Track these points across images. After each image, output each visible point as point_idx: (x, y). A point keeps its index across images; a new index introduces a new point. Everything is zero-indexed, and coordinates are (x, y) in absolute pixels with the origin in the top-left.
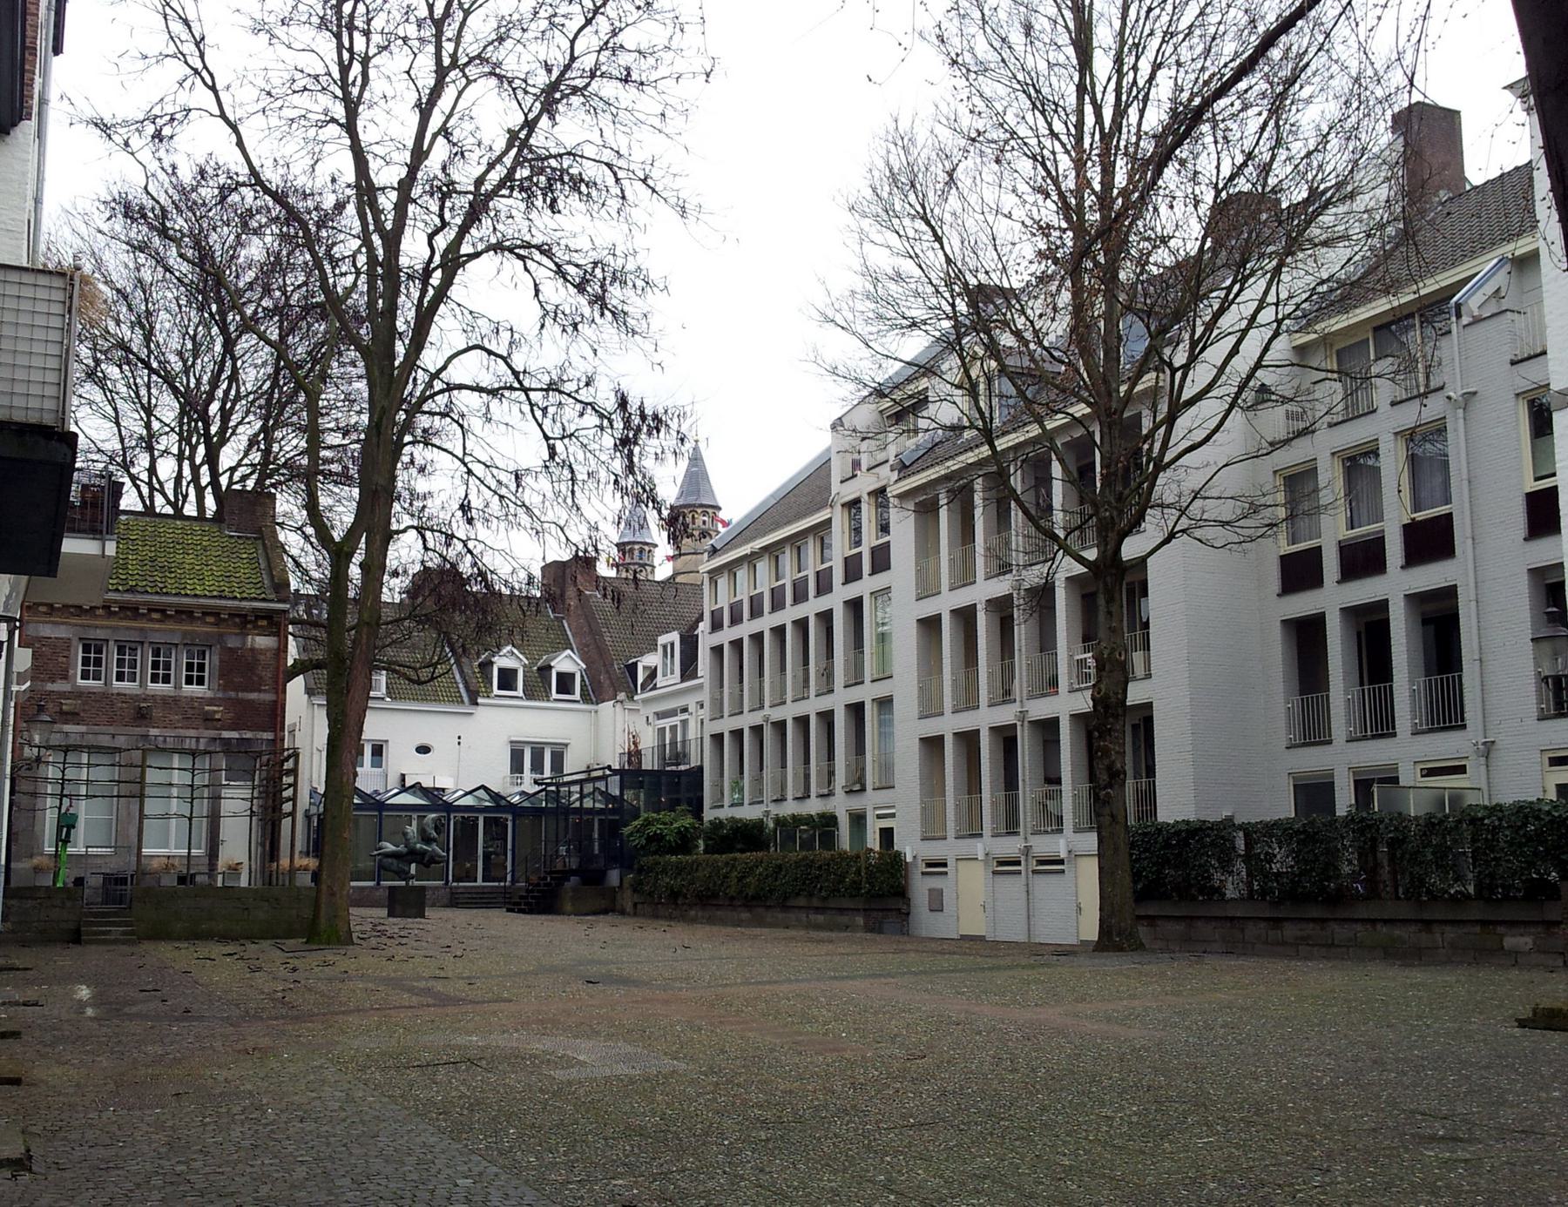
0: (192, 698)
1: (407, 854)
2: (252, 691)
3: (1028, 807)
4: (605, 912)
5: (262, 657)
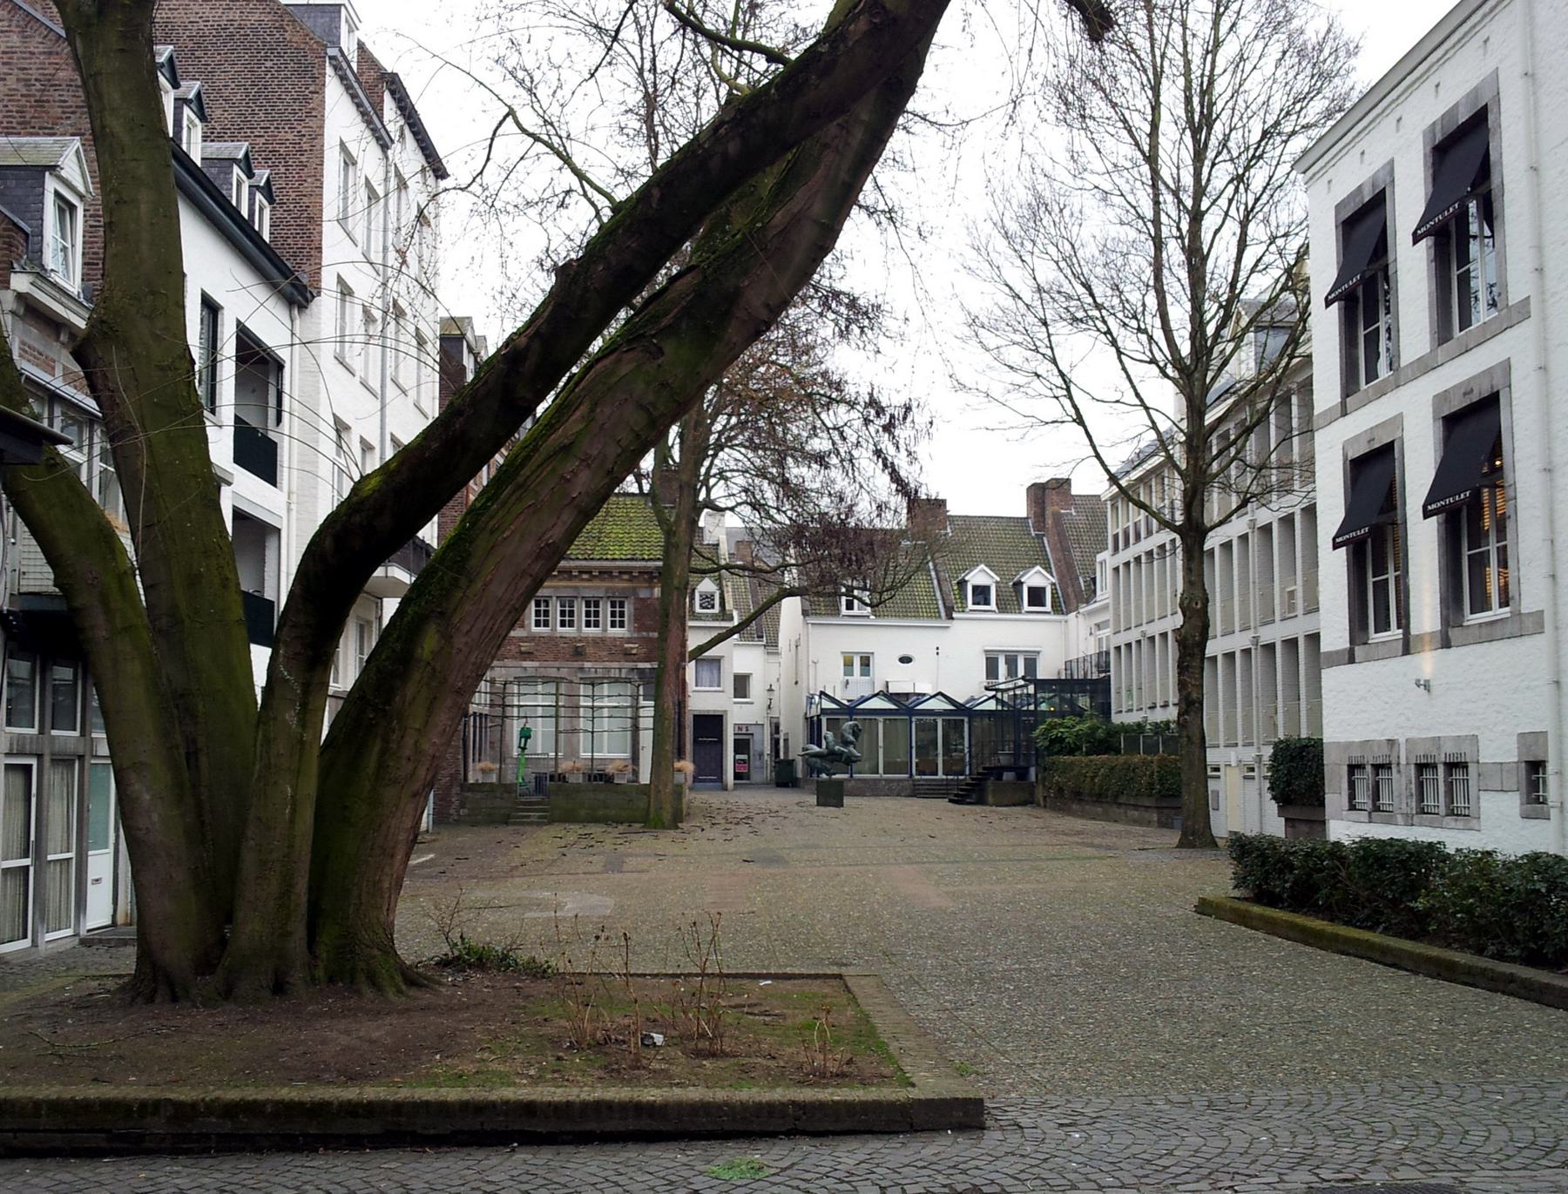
1: (828, 754)
4: (1024, 803)
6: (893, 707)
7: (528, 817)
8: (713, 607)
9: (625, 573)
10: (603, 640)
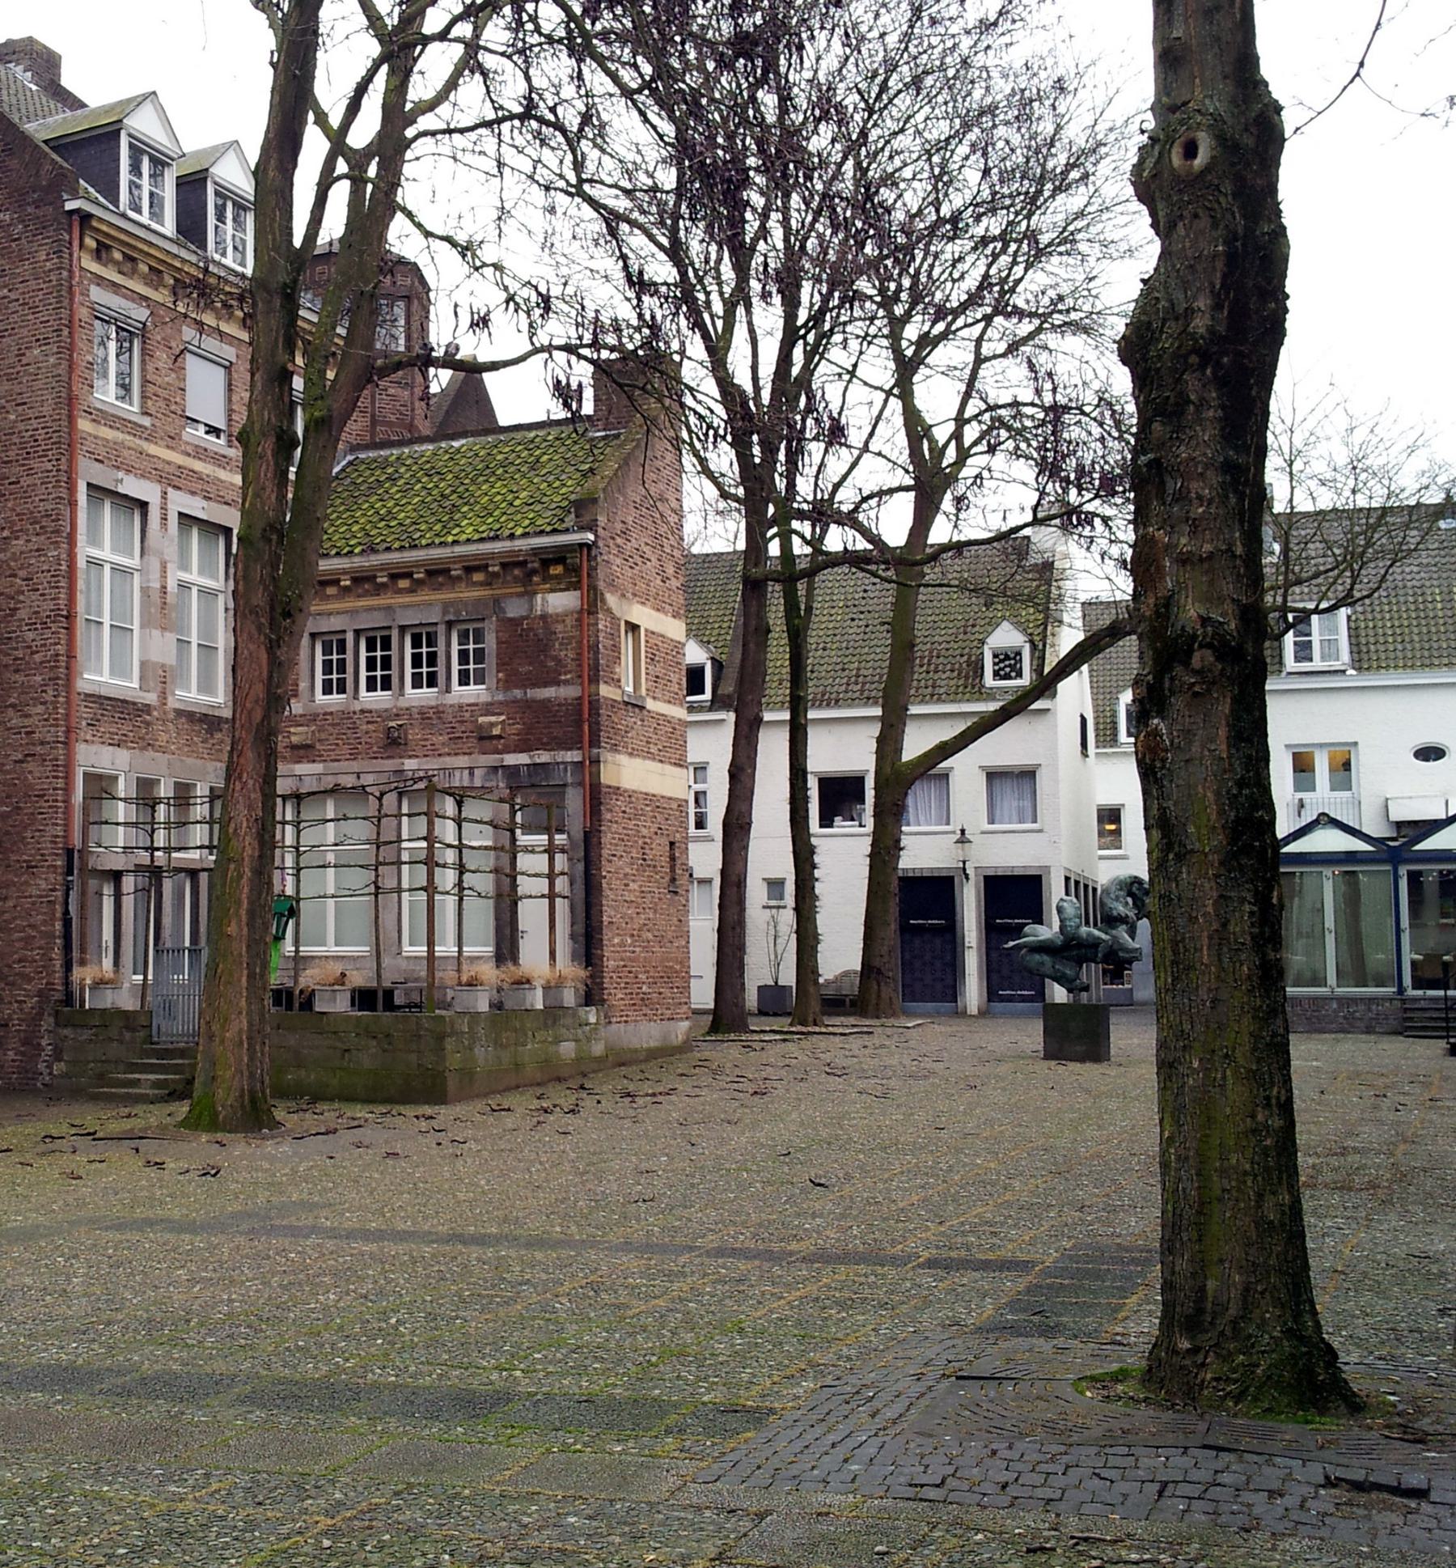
0: (461, 707)
2: (546, 685)
3: (203, 929)
5: (560, 627)
6: (1417, 847)
7: (136, 1083)
8: (1020, 675)
9: (477, 569)
10: (439, 711)
